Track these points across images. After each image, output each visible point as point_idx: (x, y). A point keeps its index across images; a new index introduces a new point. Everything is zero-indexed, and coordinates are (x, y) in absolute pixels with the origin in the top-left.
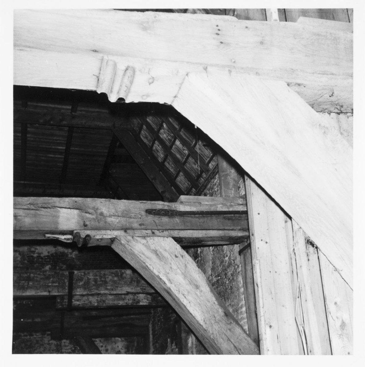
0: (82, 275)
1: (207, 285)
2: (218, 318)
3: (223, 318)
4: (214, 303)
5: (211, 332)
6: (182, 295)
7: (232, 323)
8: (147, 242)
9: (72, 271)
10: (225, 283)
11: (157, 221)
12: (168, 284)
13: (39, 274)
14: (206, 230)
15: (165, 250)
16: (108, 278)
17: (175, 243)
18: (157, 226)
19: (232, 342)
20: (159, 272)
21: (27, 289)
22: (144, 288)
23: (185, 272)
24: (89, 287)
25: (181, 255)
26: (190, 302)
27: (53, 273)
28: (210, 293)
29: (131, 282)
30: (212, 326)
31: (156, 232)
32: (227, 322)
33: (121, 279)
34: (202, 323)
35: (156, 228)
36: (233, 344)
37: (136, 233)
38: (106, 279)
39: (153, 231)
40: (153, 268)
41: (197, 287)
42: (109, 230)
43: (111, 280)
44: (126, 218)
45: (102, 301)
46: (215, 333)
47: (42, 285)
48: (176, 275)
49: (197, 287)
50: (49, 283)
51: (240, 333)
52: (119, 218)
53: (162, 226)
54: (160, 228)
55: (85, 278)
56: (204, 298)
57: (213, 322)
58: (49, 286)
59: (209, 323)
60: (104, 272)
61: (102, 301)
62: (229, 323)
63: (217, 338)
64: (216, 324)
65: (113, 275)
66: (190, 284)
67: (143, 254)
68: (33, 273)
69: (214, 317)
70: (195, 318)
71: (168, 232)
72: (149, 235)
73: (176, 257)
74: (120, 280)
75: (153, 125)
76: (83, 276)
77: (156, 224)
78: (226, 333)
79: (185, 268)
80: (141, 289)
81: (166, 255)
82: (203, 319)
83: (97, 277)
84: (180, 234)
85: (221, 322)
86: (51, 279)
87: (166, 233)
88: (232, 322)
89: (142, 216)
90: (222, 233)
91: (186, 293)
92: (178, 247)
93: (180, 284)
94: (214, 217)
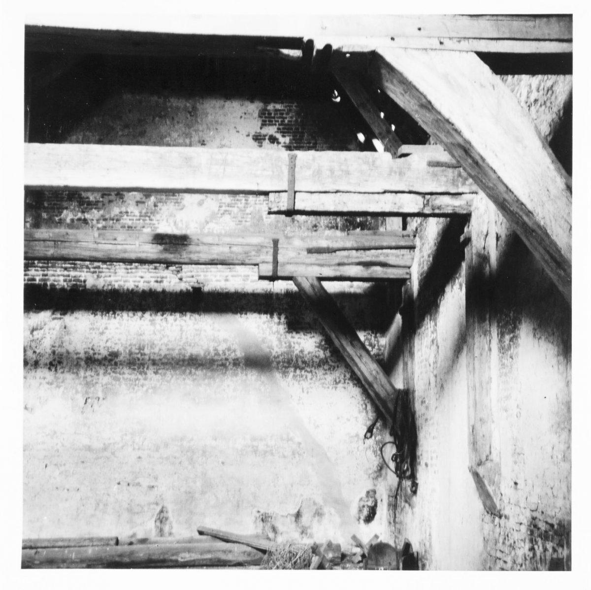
4: (548, 167)
5: (541, 215)
10: (528, 235)
22: (411, 184)
24: (320, 179)
26: (504, 165)
29: (390, 174)
30: (543, 206)
31: (448, 43)
33: (373, 168)
57: (545, 199)
59: (538, 201)
63: (551, 226)
71: (469, 43)
74: (372, 170)
75: (377, 256)
77: (447, 28)
85: (559, 199)
87: (465, 45)
92: (486, 68)
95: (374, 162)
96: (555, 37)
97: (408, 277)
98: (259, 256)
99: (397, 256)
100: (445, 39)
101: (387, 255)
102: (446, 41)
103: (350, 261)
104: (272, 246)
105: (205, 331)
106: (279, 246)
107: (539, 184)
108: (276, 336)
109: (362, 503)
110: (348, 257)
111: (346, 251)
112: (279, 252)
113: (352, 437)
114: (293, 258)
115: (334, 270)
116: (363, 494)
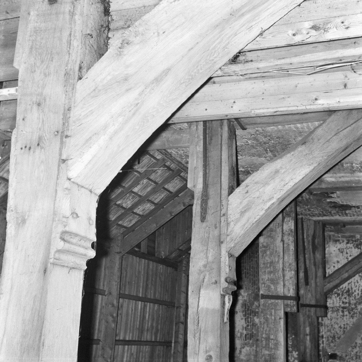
0: (264, 286)
2: (307, 152)
4: (293, 155)
11: (213, 211)
13: (263, 329)
14: (221, 162)
15: (241, 203)
18: (217, 211)
20: (263, 209)
21: (277, 341)
26: (292, 179)
27: (262, 315)
28: (283, 159)
29: (272, 237)
31: (222, 212)
32: (311, 142)
34: (312, 168)
35: (219, 212)
36: (333, 136)
39: (222, 215)
40: (258, 215)
41: (277, 172)
49: (277, 172)
50: (272, 319)
51: (322, 129)
52: (209, 248)
54: (219, 208)
55: (268, 283)
57: (311, 156)
58: (275, 319)
65: (265, 255)
68: (262, 335)
69: (306, 155)
72: (226, 219)
73: (247, 192)
76: (266, 285)
81: (245, 202)
86: (268, 316)
87: (224, 203)
89: (207, 226)
93: (274, 189)
94: (209, 154)
95: (264, 247)
96: (220, 153)
97: (321, 223)
98: (312, 316)
99: (308, 230)
100: (221, 213)
101: (308, 235)
102: (222, 212)
103: (312, 258)
104: (305, 308)
105: (357, 352)
106: (305, 303)
107: (303, 160)
108: (358, 305)
110: (310, 260)
111: (306, 261)
112: (308, 303)
114: (312, 295)
115: (319, 268)
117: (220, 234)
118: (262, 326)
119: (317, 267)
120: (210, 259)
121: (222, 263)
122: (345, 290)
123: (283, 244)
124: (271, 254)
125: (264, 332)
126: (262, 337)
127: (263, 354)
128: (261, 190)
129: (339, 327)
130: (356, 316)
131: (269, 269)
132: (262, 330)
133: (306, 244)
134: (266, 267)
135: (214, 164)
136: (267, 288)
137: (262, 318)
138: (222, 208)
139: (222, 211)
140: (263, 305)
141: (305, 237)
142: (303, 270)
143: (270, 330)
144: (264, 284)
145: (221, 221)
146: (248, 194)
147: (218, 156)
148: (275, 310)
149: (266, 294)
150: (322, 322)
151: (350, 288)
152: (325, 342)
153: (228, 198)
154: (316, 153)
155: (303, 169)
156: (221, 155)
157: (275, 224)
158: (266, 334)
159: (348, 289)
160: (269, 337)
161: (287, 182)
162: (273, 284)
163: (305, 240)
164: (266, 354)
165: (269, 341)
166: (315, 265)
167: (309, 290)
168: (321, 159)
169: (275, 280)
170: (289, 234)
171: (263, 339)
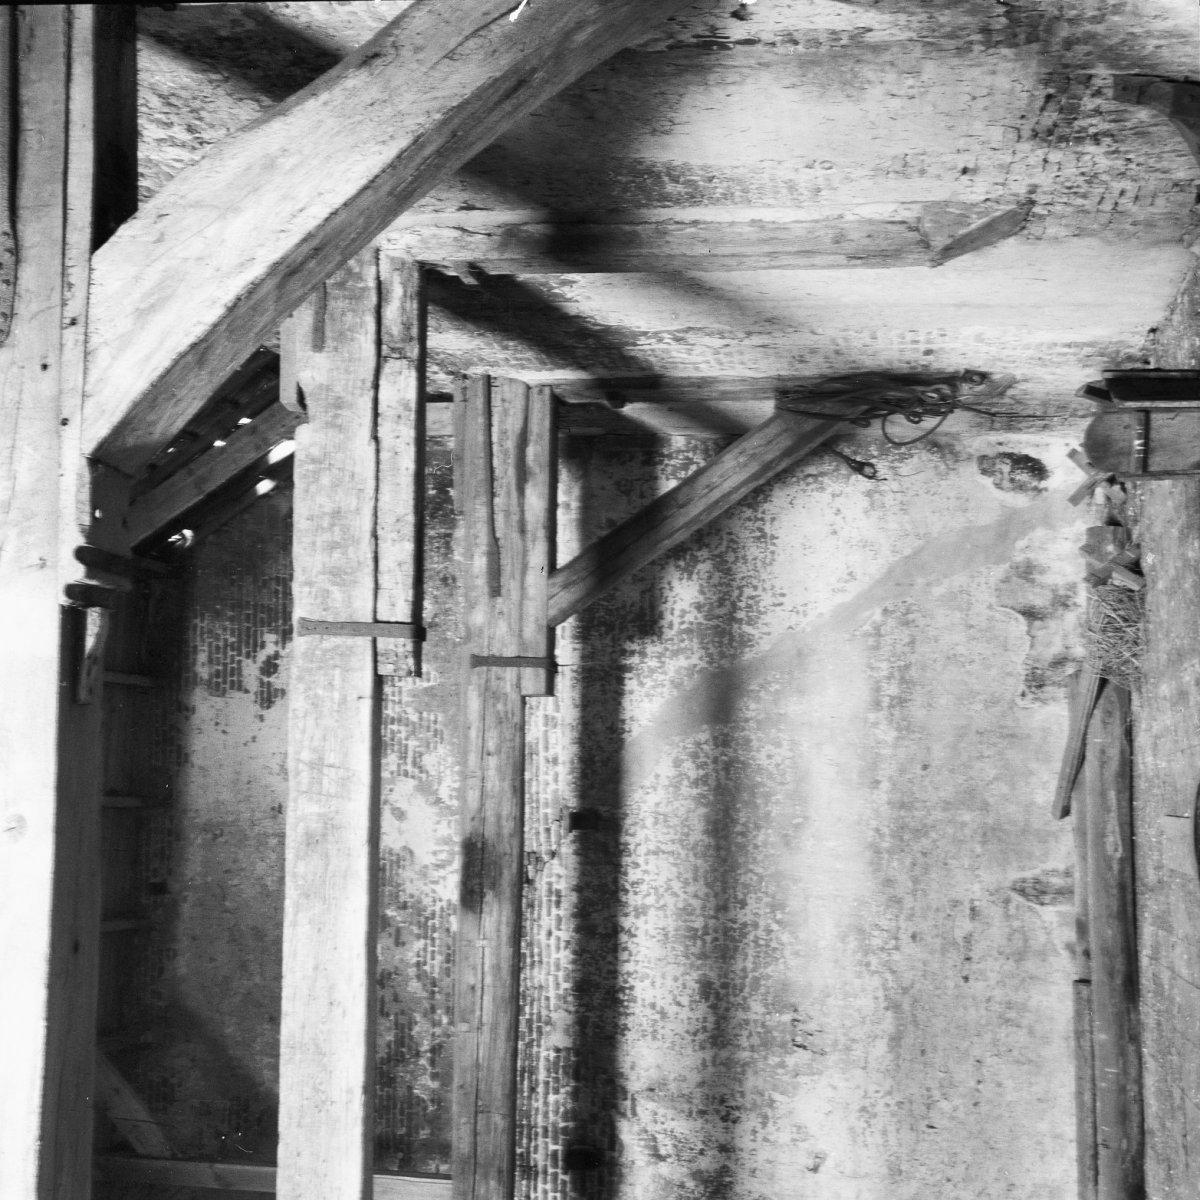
0: (310, 593)
1: (264, 127)
2: (374, 92)
3: (376, 72)
4: (325, 104)
6: (295, 220)
7: (394, 42)
8: (106, 343)
9: (94, 582)
11: (34, 307)
12: (257, 271)
13: (304, 732)
14: (67, 123)
15: (137, 278)
16: (321, 506)
17: (113, 239)
18: (49, 308)
19: (460, 44)
20: (214, 302)
21: (348, 769)
23: (216, 207)
25: (155, 223)
26: (320, 194)
27: (301, 687)
28: (290, 119)
29: (340, 428)
31: (72, 310)
32: (390, 58)
34: (390, 152)
35: (58, 309)
36: (467, 38)
37: (71, 385)
38: (324, 514)
39: (68, 321)
40: (199, 323)
41: (270, 165)
42: (57, 483)
43: (329, 497)
44: (20, 420)
45: (398, 527)
46: (427, 106)
47: (337, 721)
48: (223, 241)
49: (270, 165)
50: (332, 699)
51: (430, 11)
52: (19, 444)
53: (52, 289)
54: (56, 298)
55: (323, 581)
56: (305, 141)
57: (388, 111)
58: (344, 701)
60: (303, 521)
61: (398, 527)
62: (392, 51)
64: (397, 100)
65: (313, 488)
66: (257, 189)
67: (148, 358)
68: (298, 753)
69: (372, 104)
70: (377, 177)
72: (82, 337)
73: (159, 240)
76: (314, 590)
78: (429, 65)
79: (202, 206)
80: (361, 395)
81: (153, 275)
82: (377, 148)
83: (318, 544)
84: (80, 224)
86: (320, 692)
87: (77, 275)
88: (392, 39)
89: (13, 363)
90: (81, 64)
91: (289, 207)
92: (125, 231)
93: (256, 228)
94: (26, 93)
95: (314, 461)
96: (61, 89)
97: (547, 391)
99: (505, 412)
101: (504, 432)
102: (70, 312)
103: (515, 508)
106: (485, 654)
109: (1006, 484)
110: (507, 514)
113: (872, 504)
115: (534, 541)
116: (988, 481)
117: (61, 392)
118: (300, 725)
119: (529, 535)
120: (25, 480)
121: (63, 496)
122: (631, 612)
123: (378, 451)
124: (336, 485)
125: (306, 743)
126: (299, 760)
127: (299, 813)
128: (210, 232)
129: (607, 728)
130: (661, 694)
131: (327, 536)
132: (298, 736)
133: (496, 462)
134: (319, 528)
135: (40, 132)
136: (319, 601)
137: (301, 698)
138: (68, 295)
139: (67, 308)
140: (305, 654)
141: (495, 438)
142: (484, 548)
143: (324, 739)
144: (309, 584)
145: (61, 345)
146: (161, 248)
147: (55, 103)
148: (346, 670)
149: (316, 617)
150: (556, 714)
151: (646, 605)
152: (561, 778)
153: (90, 260)
154: (407, 100)
155: (359, 157)
156: (68, 98)
157: (351, 383)
158: (314, 750)
159: (641, 608)
160: (321, 759)
161: (301, 206)
162: (342, 584)
163: (495, 448)
164: (311, 814)
165: (320, 771)
166: (523, 531)
167: (501, 613)
168: (422, 120)
169: (346, 573)
170: (399, 417)
171: (301, 766)
